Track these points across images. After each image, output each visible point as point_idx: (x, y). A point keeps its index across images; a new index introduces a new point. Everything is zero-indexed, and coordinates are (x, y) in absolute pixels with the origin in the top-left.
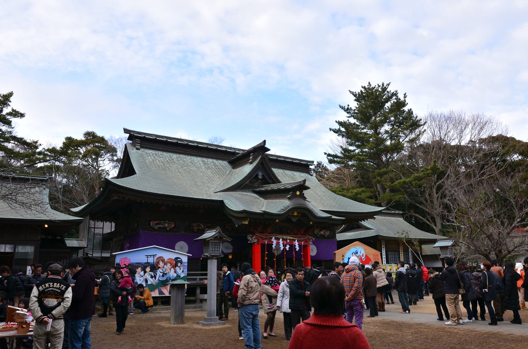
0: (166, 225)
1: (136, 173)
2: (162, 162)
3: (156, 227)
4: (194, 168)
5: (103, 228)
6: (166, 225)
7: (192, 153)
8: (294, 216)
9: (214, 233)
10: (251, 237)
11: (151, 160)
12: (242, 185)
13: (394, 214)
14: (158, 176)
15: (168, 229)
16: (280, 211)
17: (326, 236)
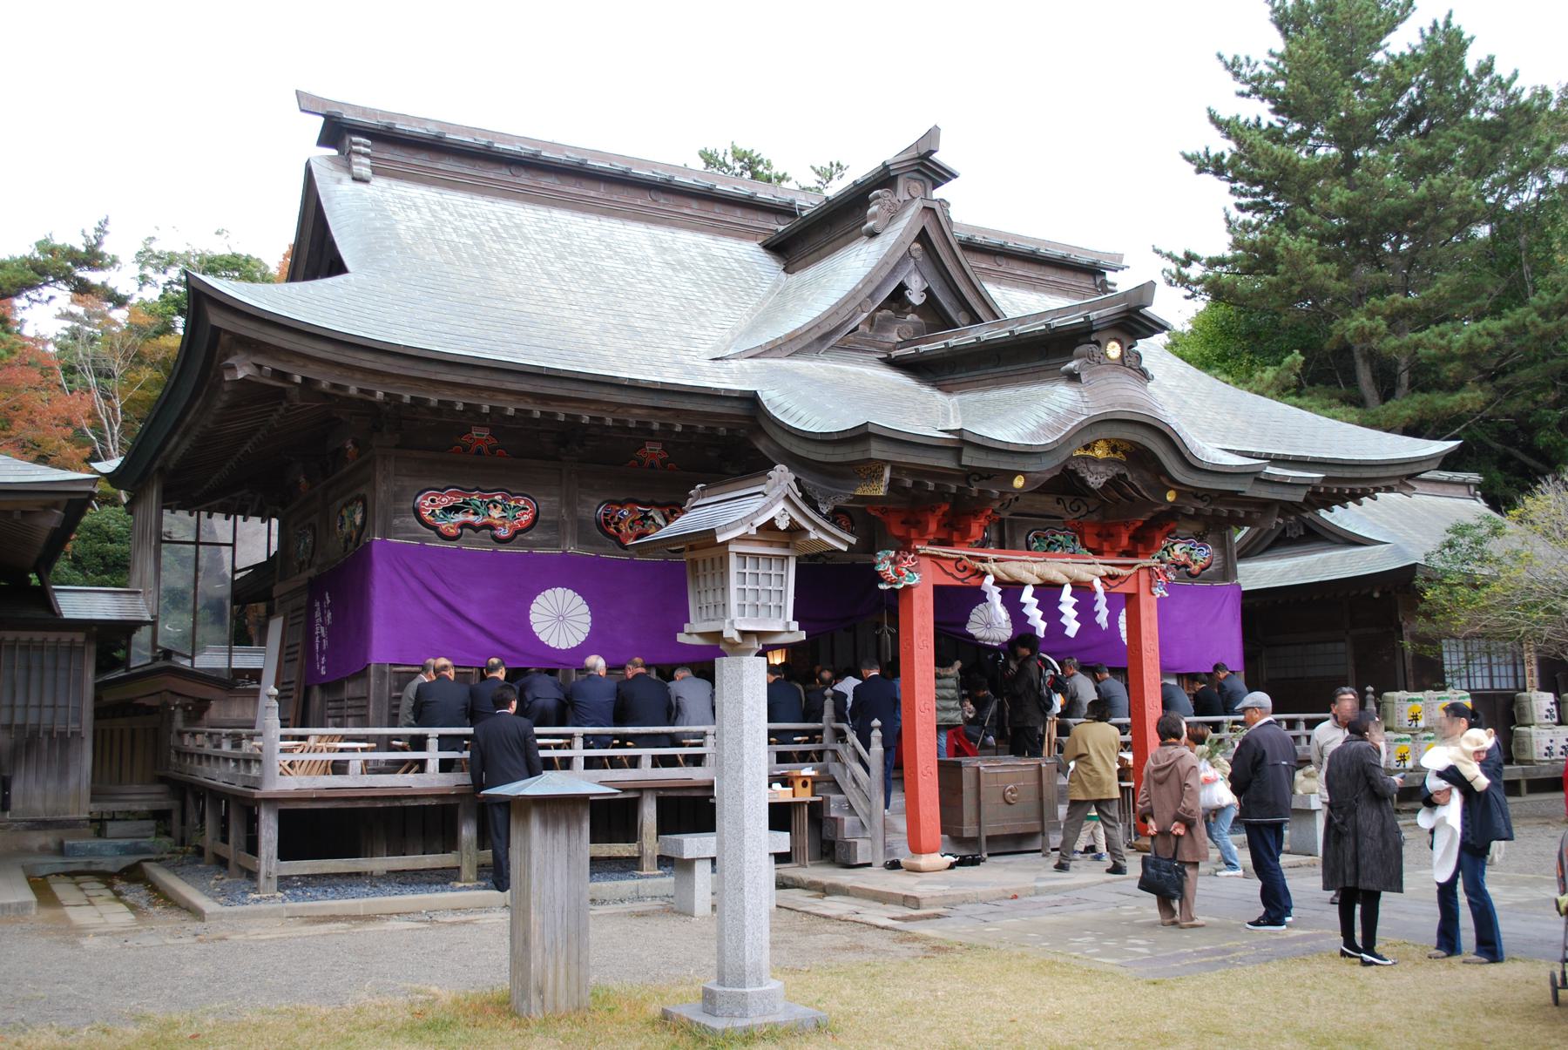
0: (496, 513)
2: (472, 235)
3: (450, 523)
5: (233, 545)
8: (1095, 460)
10: (894, 562)
13: (1449, 482)
14: (448, 285)
15: (503, 533)
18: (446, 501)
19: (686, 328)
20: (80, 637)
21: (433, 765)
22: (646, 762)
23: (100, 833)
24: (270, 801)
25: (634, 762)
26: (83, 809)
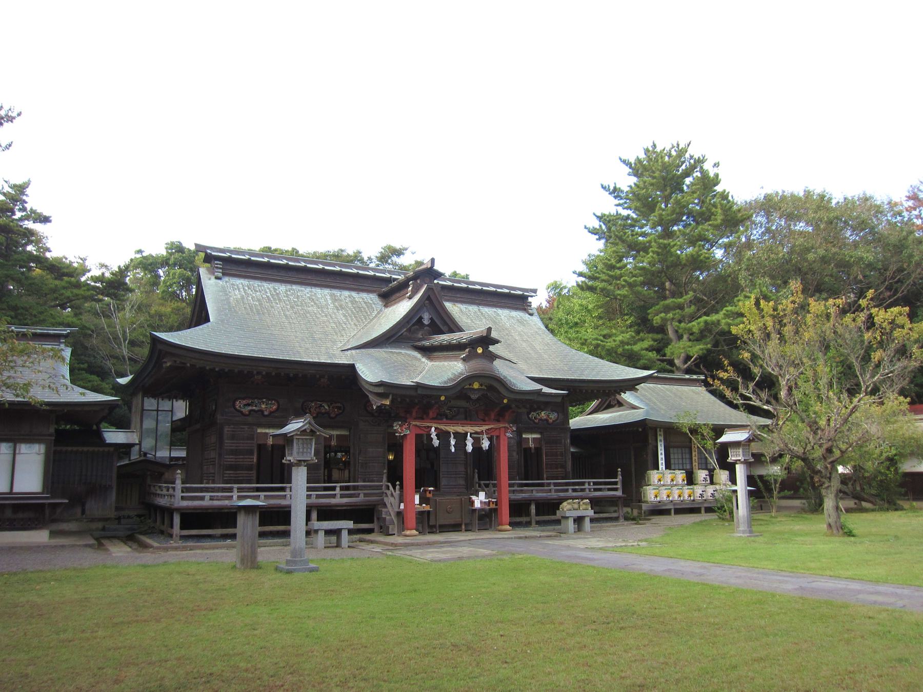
0: (263, 406)
1: (207, 320)
2: (259, 300)
3: (246, 410)
4: (315, 309)
5: (172, 411)
7: (314, 282)
8: (474, 389)
9: (301, 424)
10: (400, 426)
11: (239, 296)
12: (392, 336)
15: (266, 413)
16: (445, 382)
17: (551, 421)
19: (335, 337)
21: (235, 497)
22: (207, 498)
23: (119, 523)
24: (178, 510)
25: (202, 498)
26: (112, 514)
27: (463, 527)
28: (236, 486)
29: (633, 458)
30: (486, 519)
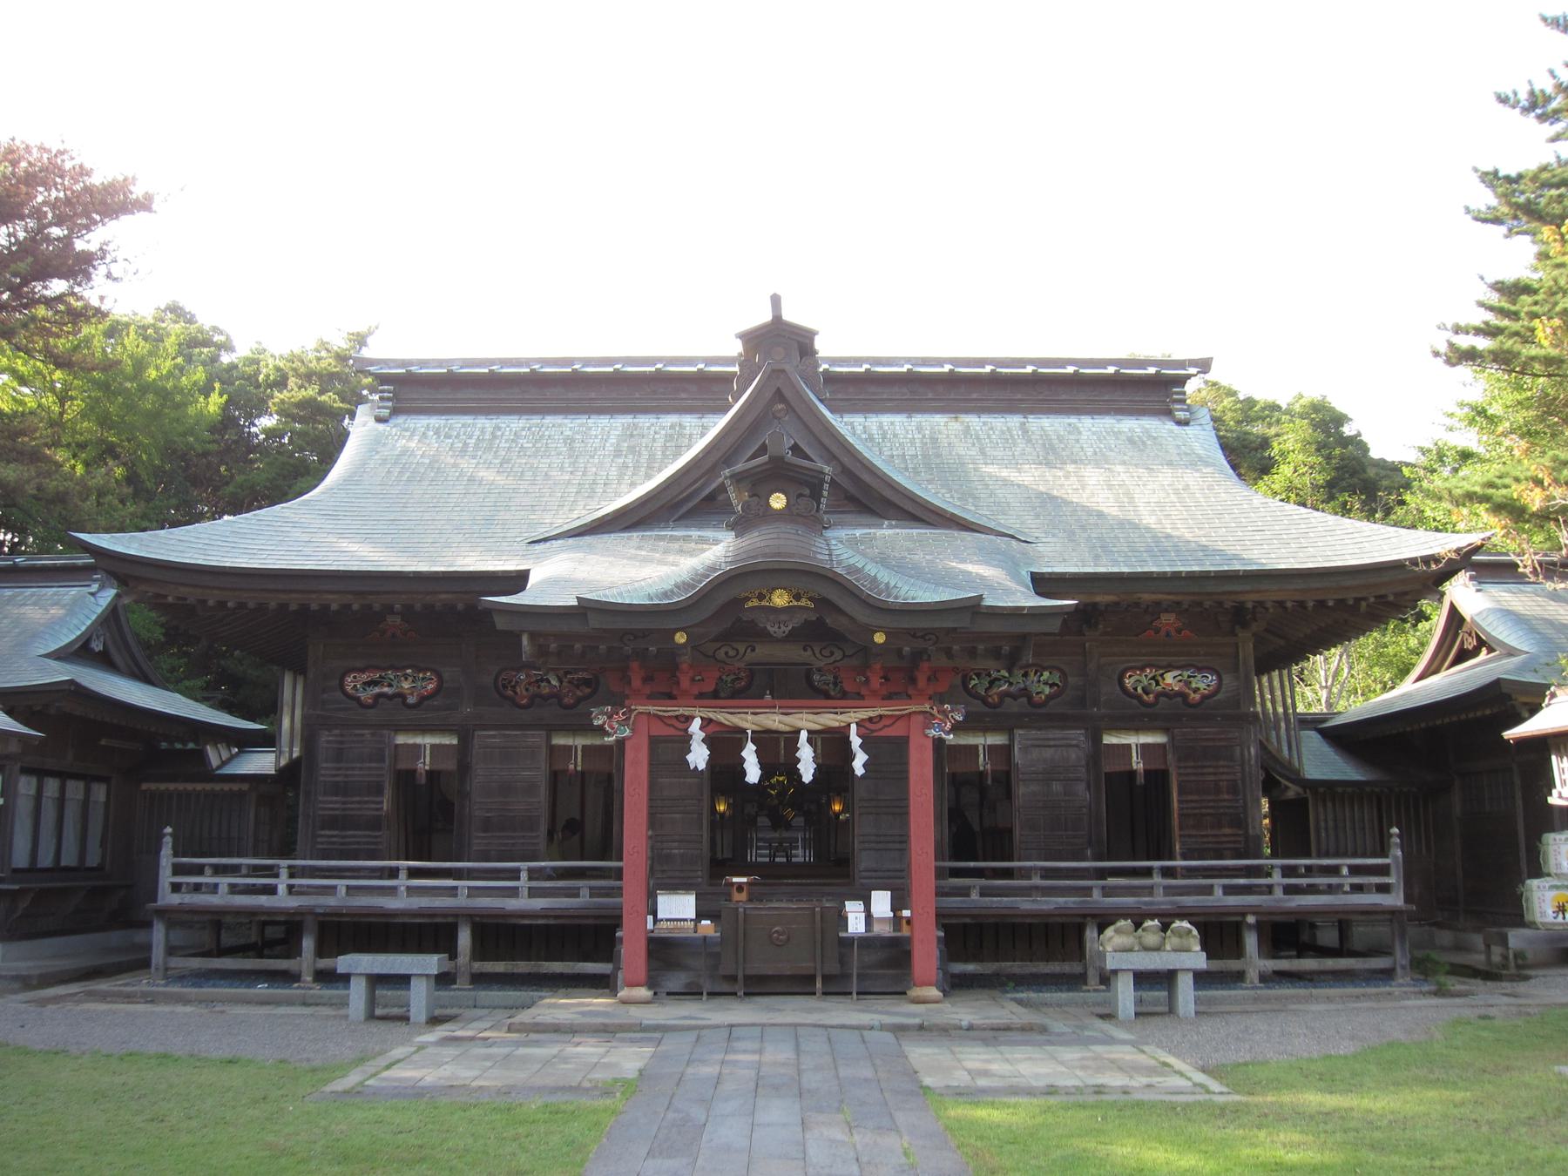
0: (406, 685)
3: (366, 695)
6: (406, 685)
15: (411, 700)
16: (666, 594)
18: (365, 677)
20: (245, 787)
21: (282, 889)
27: (819, 985)
28: (524, 865)
29: (1519, 795)
30: (884, 967)
